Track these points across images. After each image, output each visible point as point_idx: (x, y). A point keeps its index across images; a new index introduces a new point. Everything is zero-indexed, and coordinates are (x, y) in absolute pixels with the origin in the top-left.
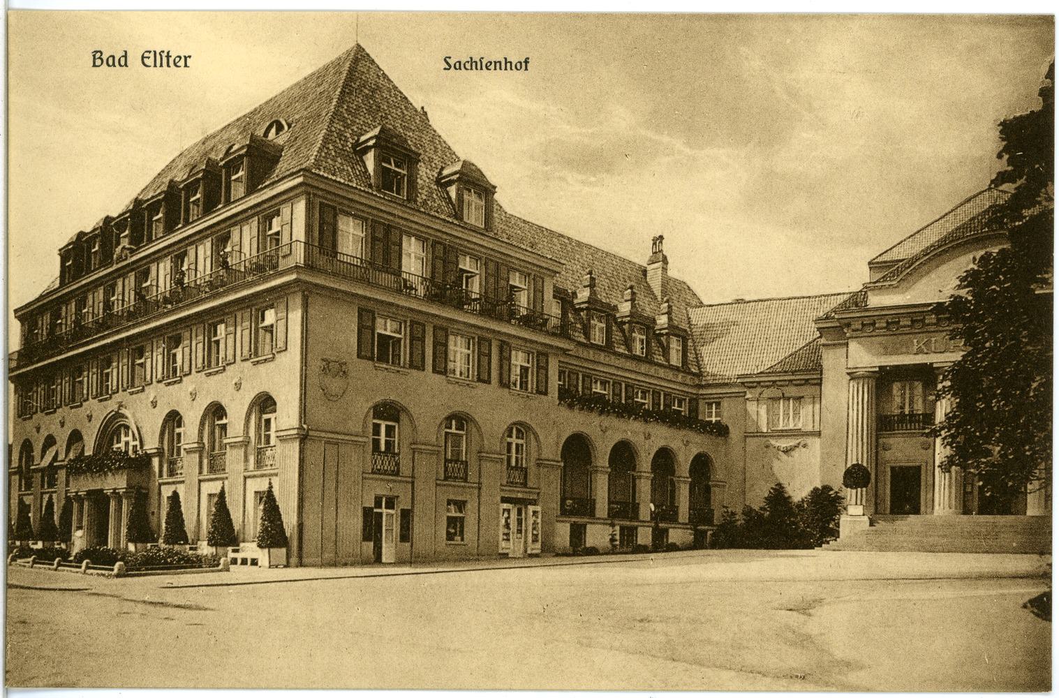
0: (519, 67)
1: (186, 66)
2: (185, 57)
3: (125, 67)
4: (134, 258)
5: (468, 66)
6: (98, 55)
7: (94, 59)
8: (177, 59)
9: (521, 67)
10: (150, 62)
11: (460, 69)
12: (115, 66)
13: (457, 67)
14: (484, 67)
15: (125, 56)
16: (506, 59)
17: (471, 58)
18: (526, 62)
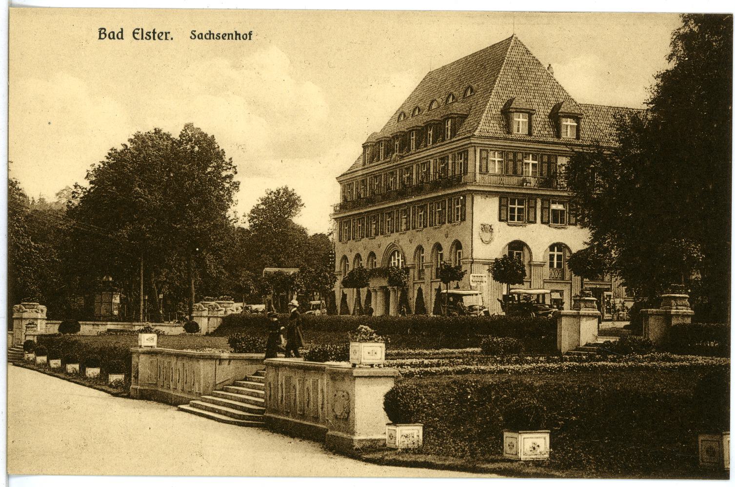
1: (166, 39)
2: (166, 33)
4: (402, 162)
5: (208, 36)
7: (100, 34)
10: (227, 37)
11: (202, 38)
13: (111, 37)
15: (122, 32)
17: (210, 31)
18: (250, 34)
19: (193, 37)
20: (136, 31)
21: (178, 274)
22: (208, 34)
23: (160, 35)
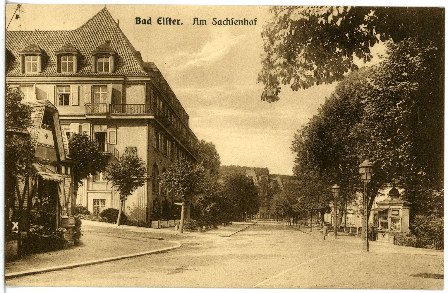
1: (178, 24)
2: (178, 20)
3: (150, 25)
5: (225, 23)
6: (138, 19)
8: (236, 22)
11: (221, 24)
13: (220, 23)
14: (233, 23)
16: (245, 19)
17: (227, 19)
19: (214, 23)
20: (160, 19)
21: (305, 25)
22: (225, 20)
23: (174, 21)
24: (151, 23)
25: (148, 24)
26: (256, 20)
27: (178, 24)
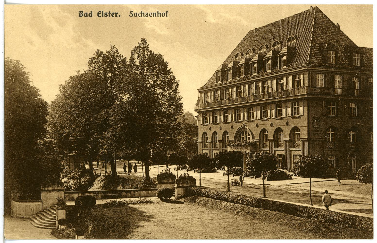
0: (163, 14)
1: (116, 16)
5: (140, 15)
6: (81, 13)
9: (165, 15)
11: (137, 16)
12: (137, 16)
16: (158, 12)
17: (142, 11)
19: (131, 15)
20: (99, 13)
22: (140, 13)
23: (113, 14)
24: (91, 16)
25: (89, 16)
26: (167, 12)
27: (116, 16)
